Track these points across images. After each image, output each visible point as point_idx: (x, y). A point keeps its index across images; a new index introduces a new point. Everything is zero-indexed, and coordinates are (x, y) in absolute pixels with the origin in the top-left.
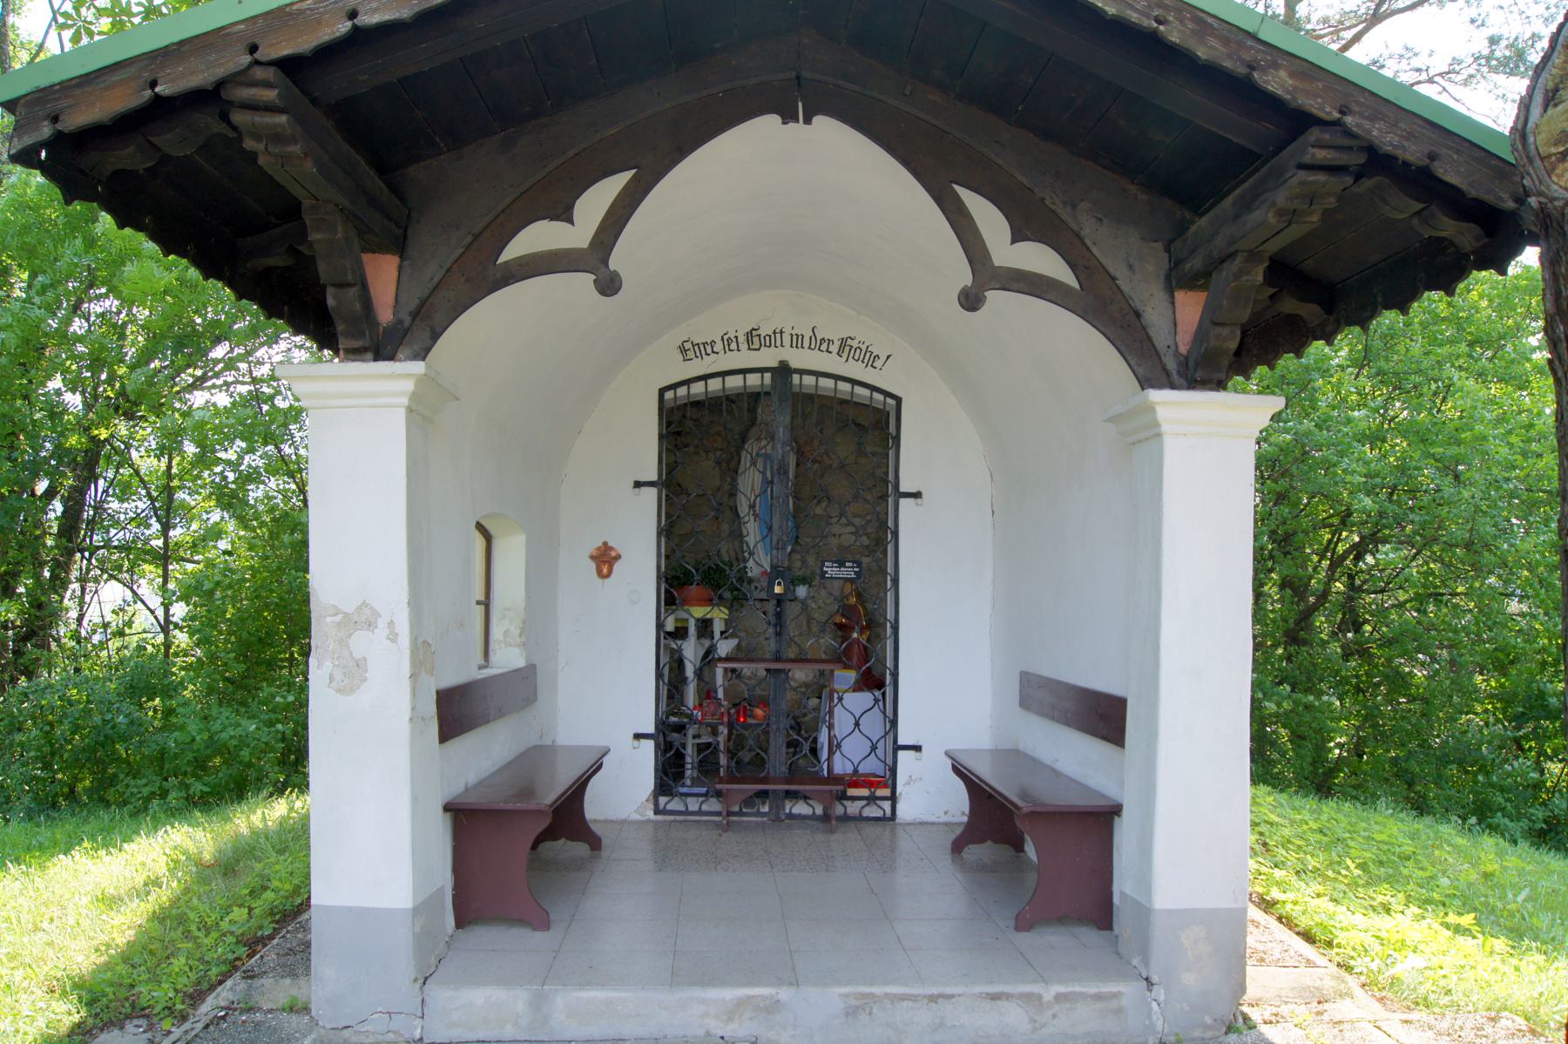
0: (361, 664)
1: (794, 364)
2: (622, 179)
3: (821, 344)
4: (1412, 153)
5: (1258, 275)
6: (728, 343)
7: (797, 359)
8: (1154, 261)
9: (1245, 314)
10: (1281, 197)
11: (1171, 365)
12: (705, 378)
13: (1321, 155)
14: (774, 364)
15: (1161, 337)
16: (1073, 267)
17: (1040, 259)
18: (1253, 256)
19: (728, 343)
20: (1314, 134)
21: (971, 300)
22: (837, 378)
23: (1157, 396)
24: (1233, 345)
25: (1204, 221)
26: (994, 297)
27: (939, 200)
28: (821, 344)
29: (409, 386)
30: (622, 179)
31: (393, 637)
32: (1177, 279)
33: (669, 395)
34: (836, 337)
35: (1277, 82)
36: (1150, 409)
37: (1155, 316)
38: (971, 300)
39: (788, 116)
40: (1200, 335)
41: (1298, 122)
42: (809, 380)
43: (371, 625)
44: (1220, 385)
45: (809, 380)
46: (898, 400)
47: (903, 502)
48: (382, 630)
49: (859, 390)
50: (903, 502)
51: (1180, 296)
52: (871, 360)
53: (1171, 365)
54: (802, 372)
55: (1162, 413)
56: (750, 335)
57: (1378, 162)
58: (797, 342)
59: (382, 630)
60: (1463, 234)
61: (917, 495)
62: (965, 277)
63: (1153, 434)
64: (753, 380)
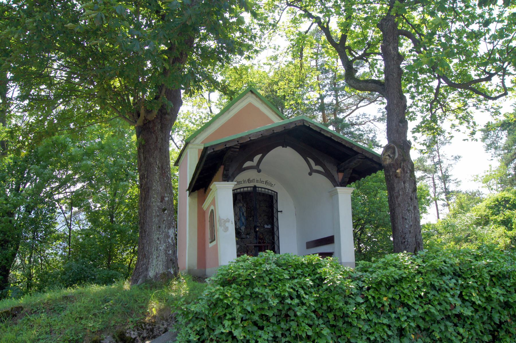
0: (227, 228)
1: (257, 186)
2: (260, 155)
3: (262, 182)
4: (370, 157)
5: (351, 171)
6: (244, 181)
7: (258, 185)
8: (335, 168)
9: (349, 176)
10: (355, 161)
11: (338, 183)
12: (240, 188)
13: (360, 157)
14: (253, 186)
15: (337, 180)
16: (324, 169)
17: (257, 158)
18: (351, 168)
19: (244, 182)
20: (359, 155)
21: (310, 174)
22: (265, 189)
23: (338, 188)
24: (347, 180)
25: (343, 163)
26: (314, 174)
27: (305, 159)
28: (262, 182)
29: (233, 186)
30: (260, 155)
31: (232, 223)
32: (339, 171)
33: (235, 191)
34: (265, 181)
35: (355, 149)
36: (336, 190)
37: (336, 176)
38: (310, 174)
39: (283, 147)
40: (343, 179)
41: (357, 153)
42: (260, 189)
43: (229, 221)
44: (345, 186)
45: (260, 189)
46: (277, 193)
47: (279, 213)
48: (230, 222)
49: (269, 191)
50: (279, 213)
51: (339, 174)
52: (271, 185)
53: (338, 183)
54: (259, 187)
55: (338, 190)
56: (248, 180)
57: (366, 158)
58: (257, 181)
59: (230, 222)
60: (377, 166)
61: (281, 211)
62: (309, 171)
63: (337, 193)
64: (249, 189)
